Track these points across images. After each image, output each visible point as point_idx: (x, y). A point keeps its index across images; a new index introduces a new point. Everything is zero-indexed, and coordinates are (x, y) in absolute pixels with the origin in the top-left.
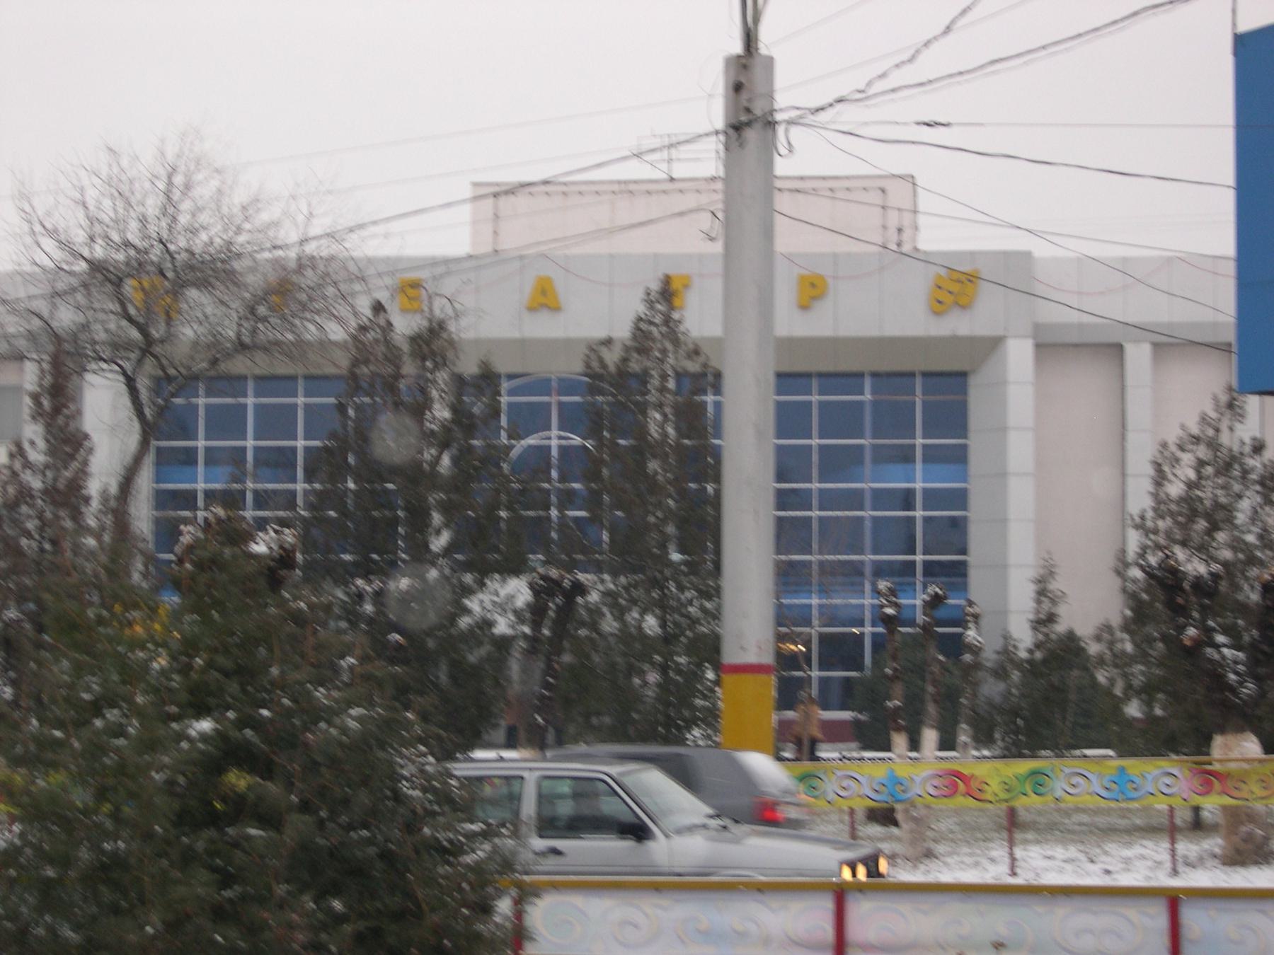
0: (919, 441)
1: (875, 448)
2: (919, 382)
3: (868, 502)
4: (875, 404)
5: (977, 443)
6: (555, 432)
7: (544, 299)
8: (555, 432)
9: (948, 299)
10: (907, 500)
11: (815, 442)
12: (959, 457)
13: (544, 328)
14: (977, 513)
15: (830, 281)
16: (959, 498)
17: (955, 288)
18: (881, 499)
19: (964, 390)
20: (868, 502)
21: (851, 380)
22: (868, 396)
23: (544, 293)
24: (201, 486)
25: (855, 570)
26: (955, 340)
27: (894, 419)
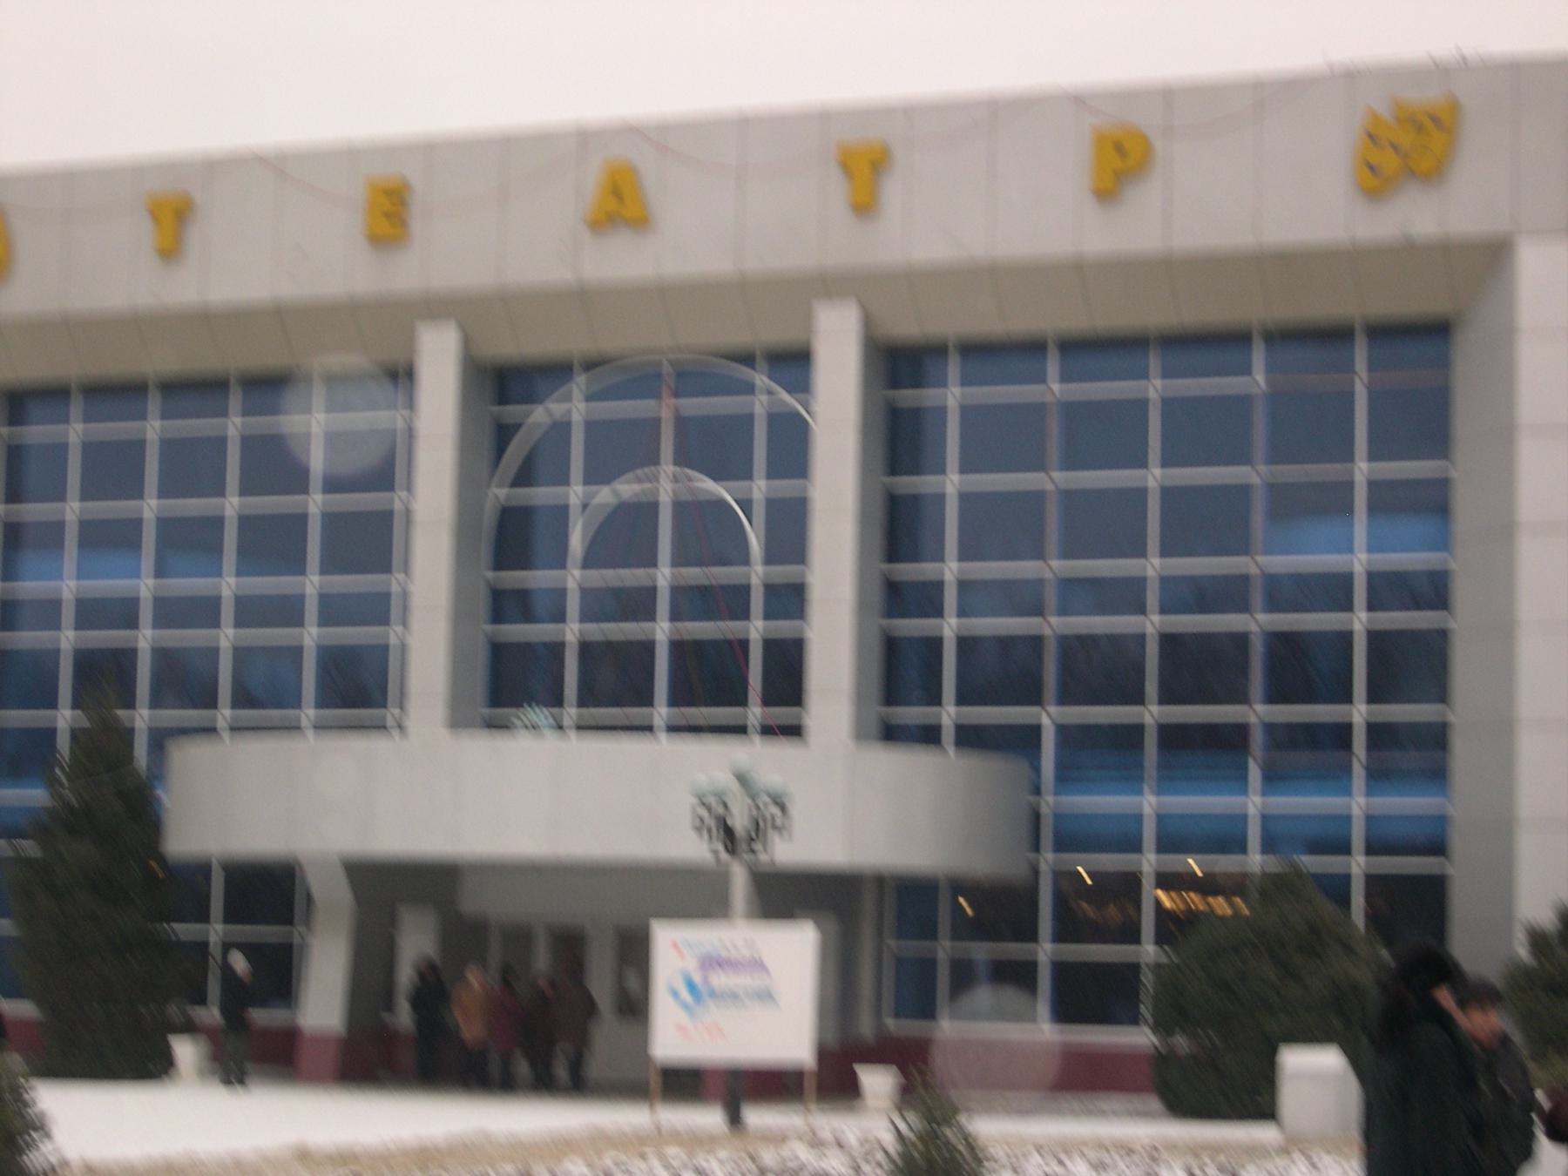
0: (1362, 469)
1: (1273, 489)
2: (1361, 353)
3: (1257, 597)
4: (1276, 397)
5: (1465, 469)
6: (668, 468)
7: (620, 204)
8: (668, 468)
9: (1389, 162)
10: (1336, 590)
11: (1154, 477)
12: (1433, 502)
13: (621, 262)
14: (1464, 621)
15: (1158, 144)
16: (1433, 591)
17: (1406, 139)
18: (1282, 593)
19: (1443, 363)
20: (1257, 597)
21: (1222, 344)
22: (1260, 377)
23: (617, 193)
24: (1360, 562)
25: (1231, 740)
26: (1408, 252)
27: (1312, 428)
